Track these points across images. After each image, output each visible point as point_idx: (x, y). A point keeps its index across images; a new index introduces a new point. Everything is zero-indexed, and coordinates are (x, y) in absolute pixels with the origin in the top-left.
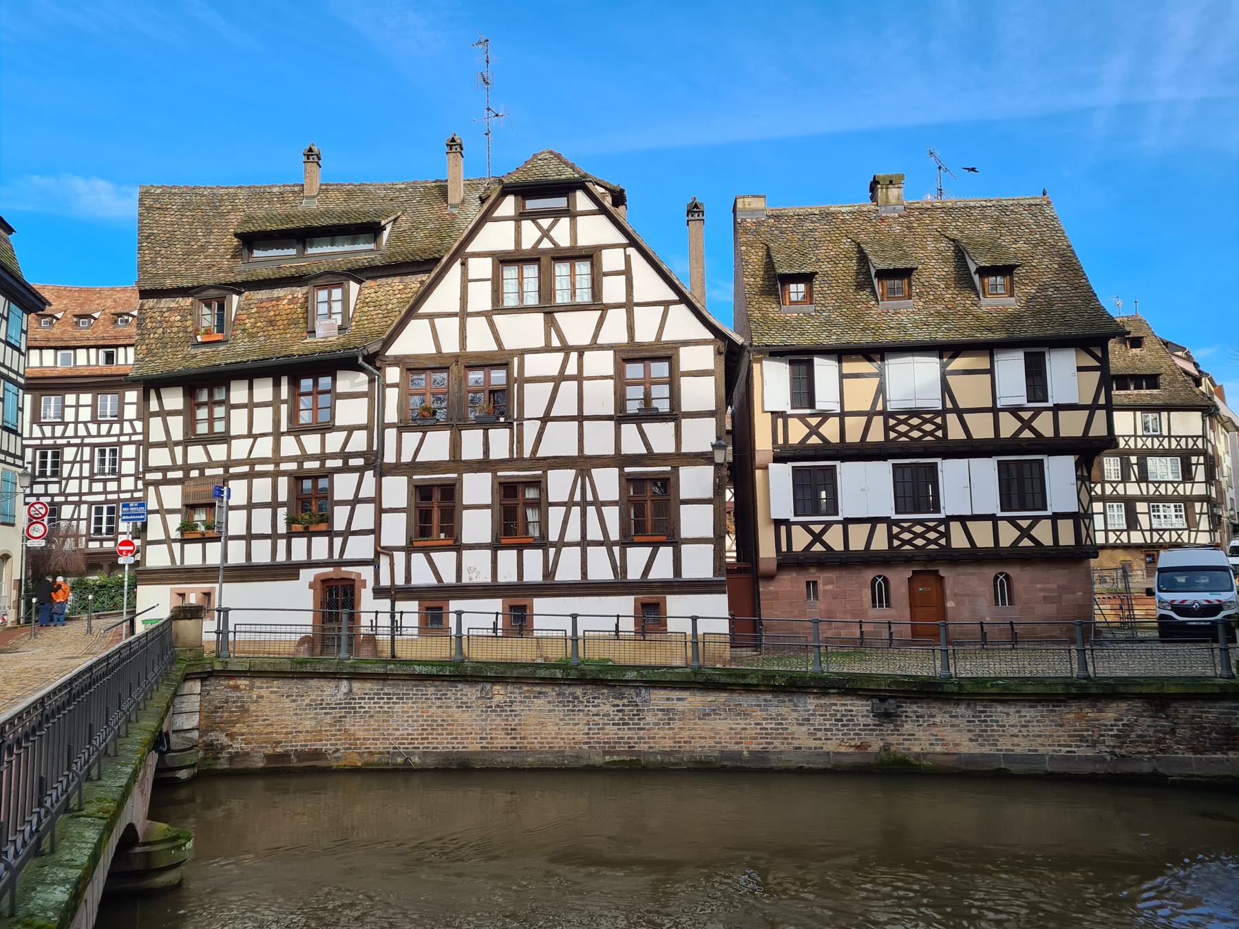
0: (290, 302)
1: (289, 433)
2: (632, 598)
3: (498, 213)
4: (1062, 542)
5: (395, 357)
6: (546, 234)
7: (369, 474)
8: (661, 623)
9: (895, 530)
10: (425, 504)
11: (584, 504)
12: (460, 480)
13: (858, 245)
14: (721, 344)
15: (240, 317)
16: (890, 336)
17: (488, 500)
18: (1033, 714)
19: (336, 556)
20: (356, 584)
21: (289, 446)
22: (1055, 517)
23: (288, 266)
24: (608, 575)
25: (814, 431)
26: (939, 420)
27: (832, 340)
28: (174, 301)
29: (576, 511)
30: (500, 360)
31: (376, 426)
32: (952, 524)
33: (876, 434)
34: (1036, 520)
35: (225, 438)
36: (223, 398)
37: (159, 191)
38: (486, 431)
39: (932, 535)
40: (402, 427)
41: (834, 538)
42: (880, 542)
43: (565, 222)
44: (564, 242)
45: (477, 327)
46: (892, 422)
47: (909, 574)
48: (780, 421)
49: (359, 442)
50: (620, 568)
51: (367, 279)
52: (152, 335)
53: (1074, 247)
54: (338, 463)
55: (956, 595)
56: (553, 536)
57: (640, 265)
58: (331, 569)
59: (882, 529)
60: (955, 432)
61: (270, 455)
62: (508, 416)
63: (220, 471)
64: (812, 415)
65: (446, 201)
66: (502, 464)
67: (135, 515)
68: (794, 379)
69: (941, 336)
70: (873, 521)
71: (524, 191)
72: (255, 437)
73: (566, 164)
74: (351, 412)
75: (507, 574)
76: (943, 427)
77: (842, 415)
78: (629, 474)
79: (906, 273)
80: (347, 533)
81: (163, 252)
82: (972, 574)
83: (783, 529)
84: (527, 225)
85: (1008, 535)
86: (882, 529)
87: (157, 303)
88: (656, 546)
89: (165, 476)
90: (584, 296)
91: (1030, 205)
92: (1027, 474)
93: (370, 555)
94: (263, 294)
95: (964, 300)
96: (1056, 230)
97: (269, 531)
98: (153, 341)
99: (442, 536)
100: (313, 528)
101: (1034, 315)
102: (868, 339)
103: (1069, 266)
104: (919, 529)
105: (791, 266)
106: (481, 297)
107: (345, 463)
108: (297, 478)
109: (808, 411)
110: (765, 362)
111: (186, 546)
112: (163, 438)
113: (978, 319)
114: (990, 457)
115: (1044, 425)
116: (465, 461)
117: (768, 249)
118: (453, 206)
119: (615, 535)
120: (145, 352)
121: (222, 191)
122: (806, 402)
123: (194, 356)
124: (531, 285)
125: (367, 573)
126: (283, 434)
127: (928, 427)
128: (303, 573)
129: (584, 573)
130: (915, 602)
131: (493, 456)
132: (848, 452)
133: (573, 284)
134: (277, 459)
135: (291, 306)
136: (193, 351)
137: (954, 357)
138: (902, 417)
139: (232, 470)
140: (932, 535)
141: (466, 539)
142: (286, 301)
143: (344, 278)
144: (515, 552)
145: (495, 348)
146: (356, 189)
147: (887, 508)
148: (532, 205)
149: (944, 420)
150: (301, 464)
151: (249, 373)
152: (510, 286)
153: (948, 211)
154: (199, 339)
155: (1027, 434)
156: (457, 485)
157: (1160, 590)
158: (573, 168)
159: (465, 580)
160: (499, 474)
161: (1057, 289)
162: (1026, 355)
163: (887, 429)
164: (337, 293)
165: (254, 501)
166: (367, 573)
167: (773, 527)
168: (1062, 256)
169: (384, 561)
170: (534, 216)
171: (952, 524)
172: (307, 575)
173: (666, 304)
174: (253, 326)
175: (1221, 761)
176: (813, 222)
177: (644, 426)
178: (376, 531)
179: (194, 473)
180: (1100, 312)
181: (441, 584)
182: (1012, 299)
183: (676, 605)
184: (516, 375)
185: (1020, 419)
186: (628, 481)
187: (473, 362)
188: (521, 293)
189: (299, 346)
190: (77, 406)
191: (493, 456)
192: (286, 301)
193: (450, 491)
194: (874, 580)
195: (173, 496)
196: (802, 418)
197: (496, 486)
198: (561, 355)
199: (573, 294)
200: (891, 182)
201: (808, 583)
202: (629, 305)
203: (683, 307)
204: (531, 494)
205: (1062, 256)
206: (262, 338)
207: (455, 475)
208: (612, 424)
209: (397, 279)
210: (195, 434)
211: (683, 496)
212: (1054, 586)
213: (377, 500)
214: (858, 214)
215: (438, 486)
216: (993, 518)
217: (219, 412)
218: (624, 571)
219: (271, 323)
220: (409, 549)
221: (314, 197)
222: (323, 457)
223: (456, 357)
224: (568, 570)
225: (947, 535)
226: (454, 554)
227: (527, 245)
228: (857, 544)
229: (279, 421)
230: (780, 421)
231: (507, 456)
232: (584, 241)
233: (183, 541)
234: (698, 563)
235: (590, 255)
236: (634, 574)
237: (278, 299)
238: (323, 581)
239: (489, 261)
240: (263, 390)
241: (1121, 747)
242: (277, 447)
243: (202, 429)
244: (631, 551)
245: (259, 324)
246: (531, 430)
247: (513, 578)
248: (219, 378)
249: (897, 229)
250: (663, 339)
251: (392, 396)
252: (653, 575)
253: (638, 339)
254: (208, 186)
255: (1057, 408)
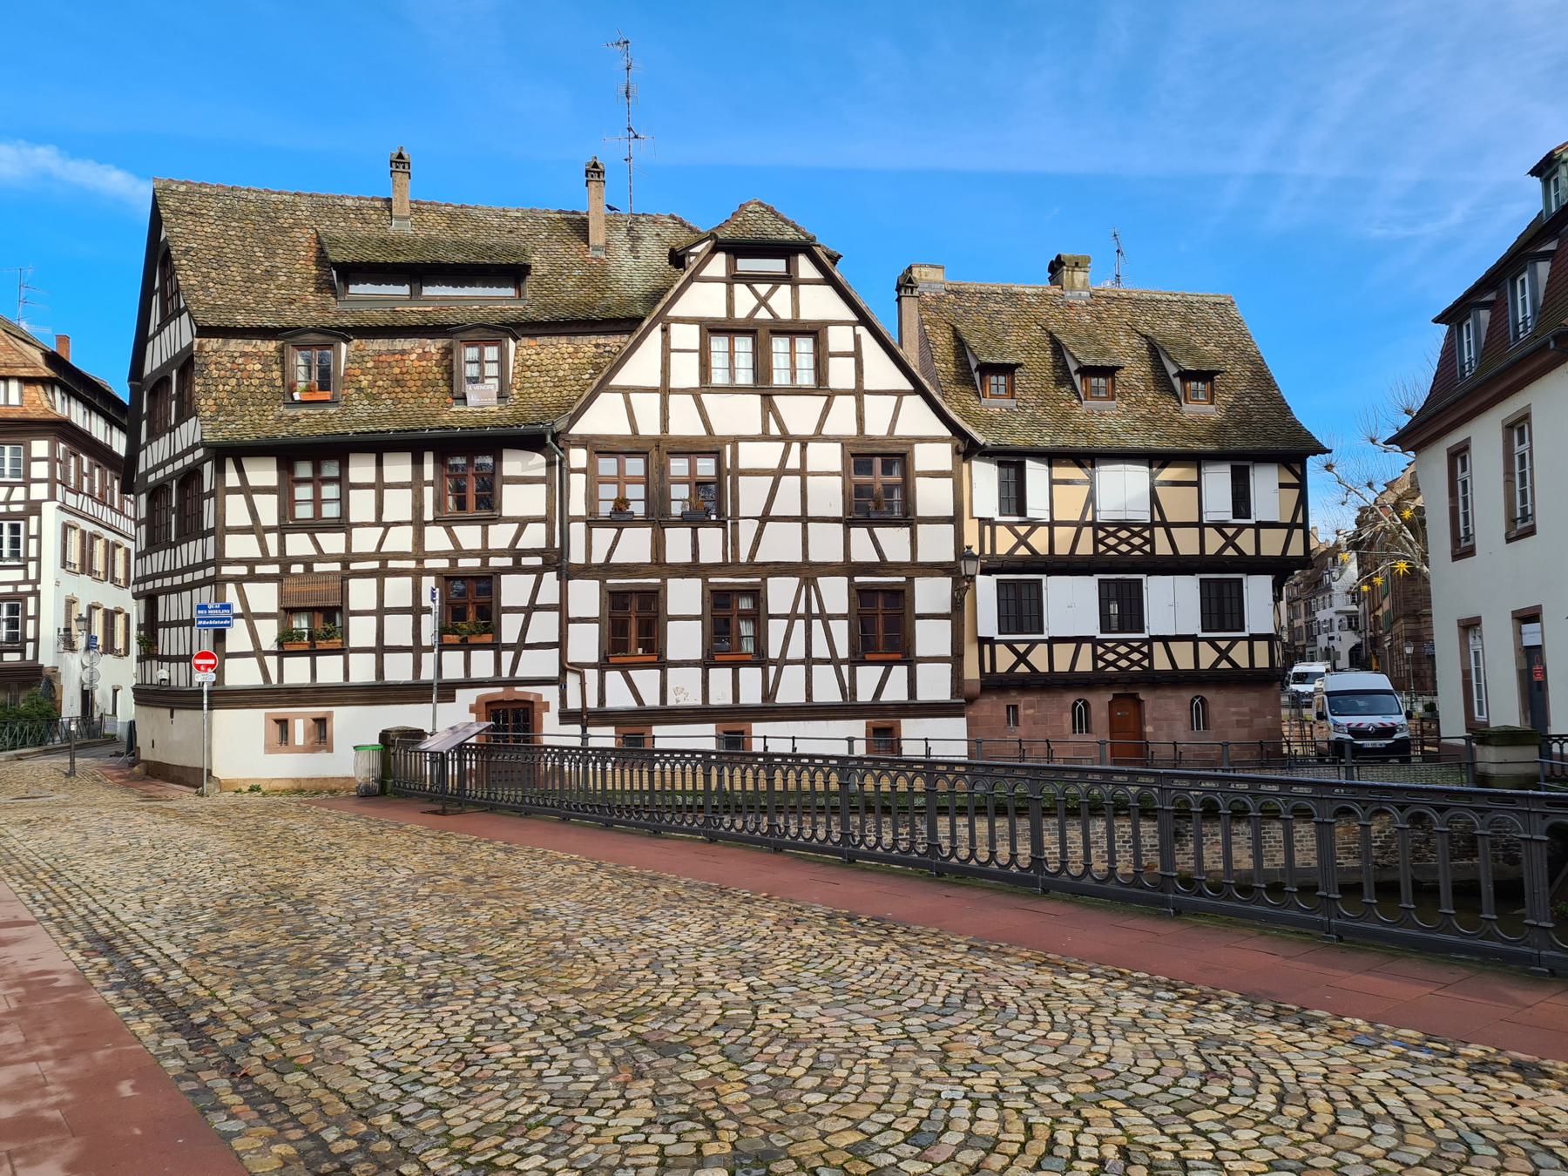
0: (421, 357)
1: (436, 522)
2: (863, 722)
3: (705, 273)
4: (1257, 665)
5: (581, 436)
6: (763, 302)
7: (550, 578)
8: (895, 746)
9: (1100, 650)
10: (619, 614)
11: (808, 617)
12: (664, 586)
13: (1050, 334)
14: (958, 442)
15: (351, 372)
16: (1104, 442)
17: (697, 610)
18: (1307, 829)
19: (505, 673)
20: (536, 707)
21: (436, 539)
22: (1253, 638)
23: (407, 309)
24: (835, 697)
25: (1022, 541)
26: (1147, 534)
27: (1045, 443)
28: (248, 344)
29: (800, 625)
30: (710, 446)
31: (556, 518)
32: (1155, 644)
33: (1085, 548)
34: (1234, 641)
35: (342, 525)
36: (336, 473)
37: (183, 188)
38: (694, 530)
39: (1136, 656)
40: (592, 521)
41: (1039, 659)
42: (1085, 664)
43: (785, 290)
44: (785, 313)
45: (682, 407)
46: (1101, 534)
47: (1110, 698)
48: (987, 529)
49: (535, 536)
50: (849, 690)
51: (524, 335)
52: (221, 387)
53: (1262, 354)
54: (508, 562)
55: (1155, 719)
56: (774, 652)
57: (869, 345)
58: (500, 690)
59: (1086, 649)
60: (1163, 548)
61: (410, 549)
62: (720, 513)
63: (337, 567)
64: (1020, 524)
65: (587, 242)
66: (866, 568)
67: (217, 619)
68: (1003, 483)
69: (1153, 444)
70: (1079, 641)
71: (736, 249)
72: (387, 526)
73: (786, 222)
74: (523, 500)
75: (721, 695)
76: (1151, 541)
77: (1052, 525)
78: (860, 584)
79: (1109, 372)
80: (520, 646)
81: (213, 274)
82: (1170, 697)
83: (987, 648)
84: (741, 290)
85: (1208, 657)
86: (1086, 649)
87: (224, 345)
88: (889, 665)
89: (252, 570)
90: (806, 378)
91: (1215, 304)
92: (1025, 595)
93: (554, 672)
94: (380, 345)
95: (1166, 405)
96: (1243, 334)
97: (410, 643)
98: (221, 395)
99: (640, 651)
100: (473, 640)
101: (1237, 425)
102: (1082, 443)
103: (1262, 377)
104: (1123, 650)
105: (991, 354)
106: (685, 372)
107: (517, 562)
108: (447, 579)
109: (1017, 519)
110: (974, 462)
111: (286, 660)
112: (248, 522)
113: (1184, 427)
114: (1192, 574)
115: (1246, 542)
116: (670, 565)
117: (955, 330)
118: (596, 248)
119: (843, 652)
120: (214, 408)
121: (274, 197)
122: (1013, 510)
123: (296, 419)
124: (744, 361)
125: (550, 694)
126: (427, 523)
127: (1137, 541)
128: (460, 694)
129: (809, 694)
130: (1115, 726)
131: (703, 559)
132: (1057, 565)
133: (793, 363)
134: (419, 553)
135: (424, 363)
136: (291, 412)
137: (1163, 466)
138: (1111, 529)
139: (353, 566)
140: (1136, 656)
141: (671, 655)
142: (414, 356)
143: (502, 334)
144: (729, 670)
145: (703, 432)
146: (458, 211)
147: (1092, 628)
148: (746, 265)
149: (1152, 534)
150: (454, 561)
151: (379, 446)
152: (718, 360)
153: (1136, 302)
154: (297, 396)
155: (1230, 552)
156: (661, 593)
157: (1333, 714)
158: (793, 226)
159: (671, 702)
160: (711, 580)
161: (1253, 399)
162: (1232, 467)
163: (1097, 541)
164: (491, 353)
165: (387, 605)
166: (550, 694)
167: (976, 645)
168: (1252, 363)
169: (572, 680)
170: (750, 279)
171: (1155, 644)
172: (466, 697)
173: (900, 394)
174: (373, 384)
175: (1465, 867)
176: (997, 303)
177: (876, 530)
178: (561, 645)
179: (297, 569)
180: (1297, 428)
181: (641, 707)
182: (1212, 407)
183: (911, 729)
184: (728, 466)
185: (1224, 535)
186: (860, 595)
187: (677, 448)
188: (732, 369)
189: (453, 416)
190: (380, 486)
191: (703, 559)
192: (414, 356)
193: (652, 600)
194: (1075, 704)
195: (264, 597)
196: (1010, 526)
197: (708, 594)
198: (781, 446)
199: (793, 376)
200: (1077, 264)
201: (1008, 707)
202: (859, 393)
203: (918, 398)
204: (745, 604)
205: (1252, 363)
206: (389, 402)
207: (658, 581)
208: (840, 527)
209: (563, 340)
210: (293, 518)
211: (918, 610)
212: (1246, 710)
213: (561, 607)
214: (1042, 296)
215: (636, 592)
216: (1193, 639)
217: (330, 491)
218: (854, 693)
219: (398, 382)
220: (603, 666)
221: (406, 218)
222: (485, 553)
223: (656, 441)
224: (791, 690)
225: (1149, 656)
226: (658, 672)
227: (741, 312)
228: (1062, 665)
229: (422, 507)
230: (987, 529)
231: (720, 560)
232: (807, 314)
233: (281, 654)
234: (935, 684)
235: (816, 332)
236: (865, 695)
237: (403, 352)
238: (488, 704)
239: (696, 328)
240: (398, 468)
241: (1382, 858)
242: (419, 539)
243: (304, 512)
244: (861, 671)
245: (380, 383)
246: (747, 531)
247: (728, 701)
248: (337, 450)
249: (1087, 319)
250: (898, 432)
251: (578, 483)
252: (886, 697)
253: (869, 431)
254: (253, 187)
255: (1260, 525)
